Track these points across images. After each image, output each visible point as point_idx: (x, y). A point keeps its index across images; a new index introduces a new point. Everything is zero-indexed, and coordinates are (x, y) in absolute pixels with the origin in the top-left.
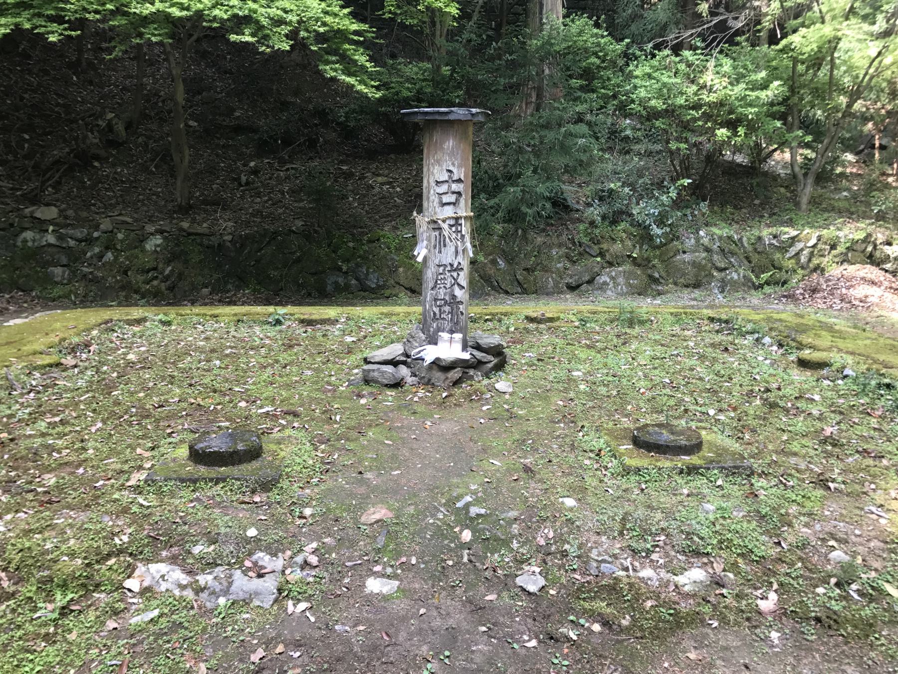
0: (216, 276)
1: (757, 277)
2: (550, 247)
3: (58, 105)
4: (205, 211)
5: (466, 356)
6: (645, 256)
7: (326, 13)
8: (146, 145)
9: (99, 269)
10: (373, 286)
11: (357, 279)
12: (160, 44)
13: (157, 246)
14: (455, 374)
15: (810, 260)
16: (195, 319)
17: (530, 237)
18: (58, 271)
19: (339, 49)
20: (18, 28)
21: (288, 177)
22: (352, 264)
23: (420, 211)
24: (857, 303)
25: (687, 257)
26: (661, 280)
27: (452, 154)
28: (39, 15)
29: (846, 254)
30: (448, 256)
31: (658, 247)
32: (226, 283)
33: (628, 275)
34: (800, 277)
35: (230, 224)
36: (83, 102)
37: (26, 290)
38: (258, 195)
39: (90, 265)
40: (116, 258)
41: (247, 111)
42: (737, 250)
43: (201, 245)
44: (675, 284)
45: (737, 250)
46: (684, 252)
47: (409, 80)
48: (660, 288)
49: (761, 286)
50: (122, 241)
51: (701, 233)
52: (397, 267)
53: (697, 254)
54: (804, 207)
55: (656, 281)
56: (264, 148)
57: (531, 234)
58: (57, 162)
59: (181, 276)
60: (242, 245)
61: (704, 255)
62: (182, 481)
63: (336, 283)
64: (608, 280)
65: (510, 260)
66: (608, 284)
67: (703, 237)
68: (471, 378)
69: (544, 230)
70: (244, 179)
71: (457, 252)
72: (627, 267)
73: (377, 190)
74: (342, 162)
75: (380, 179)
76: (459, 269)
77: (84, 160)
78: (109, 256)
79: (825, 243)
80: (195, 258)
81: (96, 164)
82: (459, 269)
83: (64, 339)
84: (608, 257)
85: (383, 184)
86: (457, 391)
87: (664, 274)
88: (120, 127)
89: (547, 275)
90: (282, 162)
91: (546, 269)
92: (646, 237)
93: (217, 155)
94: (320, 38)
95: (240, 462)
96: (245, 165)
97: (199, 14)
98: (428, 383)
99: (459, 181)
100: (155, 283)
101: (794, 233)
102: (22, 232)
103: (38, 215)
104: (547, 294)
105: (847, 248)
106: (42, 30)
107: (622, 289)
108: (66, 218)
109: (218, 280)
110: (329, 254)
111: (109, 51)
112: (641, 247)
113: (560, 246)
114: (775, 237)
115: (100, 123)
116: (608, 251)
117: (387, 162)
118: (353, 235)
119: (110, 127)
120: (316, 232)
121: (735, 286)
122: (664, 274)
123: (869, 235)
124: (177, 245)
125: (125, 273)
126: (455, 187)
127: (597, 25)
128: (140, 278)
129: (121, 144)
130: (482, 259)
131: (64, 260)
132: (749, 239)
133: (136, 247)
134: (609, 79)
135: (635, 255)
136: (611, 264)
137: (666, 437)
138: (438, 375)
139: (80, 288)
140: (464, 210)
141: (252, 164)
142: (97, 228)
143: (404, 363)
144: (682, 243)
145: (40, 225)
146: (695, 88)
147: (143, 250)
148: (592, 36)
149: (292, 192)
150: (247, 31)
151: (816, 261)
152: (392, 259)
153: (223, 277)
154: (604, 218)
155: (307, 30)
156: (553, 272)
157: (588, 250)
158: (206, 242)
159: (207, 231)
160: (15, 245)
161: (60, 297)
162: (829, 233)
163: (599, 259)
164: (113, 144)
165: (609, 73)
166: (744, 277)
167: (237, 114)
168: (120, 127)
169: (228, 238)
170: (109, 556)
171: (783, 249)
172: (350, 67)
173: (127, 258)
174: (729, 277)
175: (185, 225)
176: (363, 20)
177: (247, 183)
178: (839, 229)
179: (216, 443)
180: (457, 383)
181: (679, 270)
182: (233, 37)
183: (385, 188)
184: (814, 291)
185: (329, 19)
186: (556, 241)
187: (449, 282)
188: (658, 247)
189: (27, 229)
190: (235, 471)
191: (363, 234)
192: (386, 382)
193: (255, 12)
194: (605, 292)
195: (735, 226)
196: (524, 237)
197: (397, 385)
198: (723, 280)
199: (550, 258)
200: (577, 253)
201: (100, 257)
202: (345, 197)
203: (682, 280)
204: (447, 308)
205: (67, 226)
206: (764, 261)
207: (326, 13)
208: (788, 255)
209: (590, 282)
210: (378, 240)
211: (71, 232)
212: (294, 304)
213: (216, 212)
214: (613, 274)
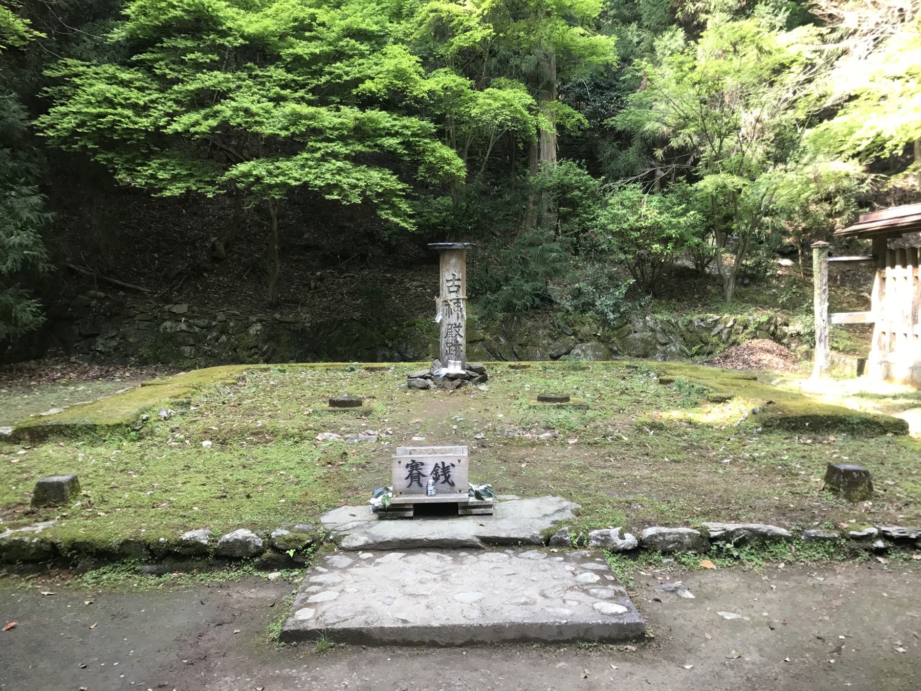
0: (299, 352)
1: (690, 350)
2: (537, 329)
3: (175, 232)
4: (289, 307)
5: (463, 372)
7: (382, 179)
8: (240, 260)
11: (399, 352)
12: (280, 200)
13: (257, 331)
14: (457, 382)
15: (729, 337)
18: (187, 349)
20: (189, 190)
21: (345, 283)
22: (396, 342)
23: (438, 296)
24: (752, 364)
25: (637, 336)
27: (455, 266)
28: (200, 181)
29: (755, 333)
30: (453, 319)
31: (616, 329)
33: (594, 349)
34: (722, 349)
35: (308, 315)
36: (192, 229)
38: (325, 296)
39: (209, 345)
40: (228, 340)
42: (674, 330)
43: (289, 330)
44: (630, 355)
45: (674, 330)
46: (635, 332)
47: (437, 210)
49: (693, 356)
51: (647, 318)
52: (428, 344)
54: (729, 299)
55: (616, 353)
56: (328, 261)
57: (524, 320)
59: (274, 351)
61: (650, 334)
65: (509, 338)
69: (533, 317)
70: (313, 285)
72: (594, 343)
73: (413, 291)
74: (387, 271)
75: (415, 283)
76: (460, 326)
77: (197, 272)
79: (739, 325)
80: (284, 339)
81: (205, 275)
84: (580, 336)
85: (419, 287)
86: (458, 390)
87: (621, 348)
88: (221, 247)
90: (341, 272)
92: (605, 322)
93: (292, 267)
94: (379, 195)
96: (312, 274)
97: (306, 184)
98: (443, 387)
99: (459, 280)
101: (716, 317)
102: (162, 323)
105: (756, 328)
106: (203, 190)
108: (193, 312)
110: (383, 332)
112: (603, 329)
113: (545, 328)
114: (702, 320)
115: (207, 244)
116: (579, 331)
117: (420, 270)
118: (396, 321)
119: (214, 247)
120: (370, 320)
121: (673, 356)
122: (621, 348)
123: (771, 319)
124: (272, 330)
125: (235, 350)
126: (456, 283)
127: (579, 166)
128: (245, 353)
131: (192, 341)
132: (683, 322)
134: (590, 206)
136: (582, 341)
138: (448, 383)
140: (462, 295)
141: (318, 273)
142: (215, 318)
143: (430, 378)
145: (176, 317)
146: (636, 217)
148: (575, 175)
149: (349, 293)
150: (335, 193)
151: (733, 338)
154: (576, 308)
155: (371, 191)
158: (292, 328)
159: (293, 320)
162: (745, 317)
164: (216, 259)
165: (590, 202)
167: (306, 236)
168: (221, 247)
171: (709, 329)
172: (397, 212)
173: (236, 340)
175: (277, 316)
176: (405, 182)
177: (315, 288)
178: (750, 315)
179: (340, 398)
180: (458, 387)
182: (327, 197)
183: (419, 289)
184: (727, 357)
185: (384, 183)
186: (541, 324)
187: (454, 333)
188: (616, 329)
189: (166, 320)
193: (340, 181)
195: (675, 313)
196: (519, 322)
197: (426, 388)
198: (664, 352)
199: (538, 337)
200: (557, 333)
202: (389, 296)
204: (453, 348)
205: (194, 318)
206: (694, 338)
207: (382, 179)
208: (713, 334)
211: (197, 322)
213: (297, 307)
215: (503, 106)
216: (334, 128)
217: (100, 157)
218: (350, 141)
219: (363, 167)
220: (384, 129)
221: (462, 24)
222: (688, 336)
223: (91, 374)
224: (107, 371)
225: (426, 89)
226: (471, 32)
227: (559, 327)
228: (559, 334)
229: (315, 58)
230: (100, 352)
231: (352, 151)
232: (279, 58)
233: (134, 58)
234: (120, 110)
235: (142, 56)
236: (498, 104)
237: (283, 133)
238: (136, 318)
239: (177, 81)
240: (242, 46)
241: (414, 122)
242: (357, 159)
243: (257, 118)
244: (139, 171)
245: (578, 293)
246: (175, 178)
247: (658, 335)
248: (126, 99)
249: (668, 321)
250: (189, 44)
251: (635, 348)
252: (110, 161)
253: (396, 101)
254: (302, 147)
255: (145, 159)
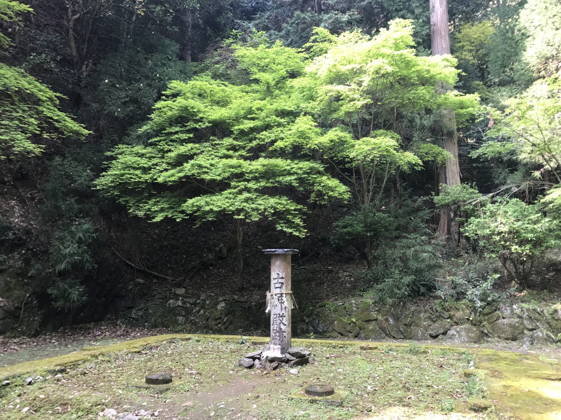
0: (246, 323)
1: (556, 336)
2: (420, 312)
6: (478, 319)
9: (197, 318)
10: (321, 331)
11: (313, 327)
13: (222, 307)
14: (275, 364)
16: (210, 339)
17: (408, 307)
18: (180, 318)
19: (286, 217)
25: (506, 321)
26: (489, 335)
27: (279, 267)
32: (250, 327)
33: (468, 331)
37: (167, 327)
40: (205, 313)
41: (286, 240)
42: (540, 318)
43: (241, 307)
44: (499, 337)
45: (540, 318)
46: (504, 318)
48: (490, 339)
50: (208, 305)
51: (514, 306)
52: (334, 321)
53: (512, 319)
58: (193, 268)
60: (260, 307)
61: (517, 320)
62: (137, 387)
63: (302, 328)
64: (455, 333)
65: (397, 319)
66: (455, 336)
67: (515, 309)
68: (283, 367)
69: (416, 303)
71: (282, 309)
72: (467, 326)
75: (345, 274)
76: (283, 316)
77: (205, 266)
78: (202, 312)
80: (238, 313)
81: (211, 268)
82: (283, 316)
83: (148, 344)
84: (455, 319)
85: (346, 276)
87: (491, 331)
89: (418, 328)
91: (418, 325)
95: (159, 384)
99: (282, 278)
100: (220, 325)
103: (177, 292)
104: (418, 340)
106: (175, 217)
107: (464, 339)
108: (188, 293)
109: (247, 325)
111: (196, 224)
113: (425, 312)
116: (454, 315)
125: (208, 320)
126: (280, 280)
127: (471, 187)
128: (214, 323)
129: (224, 258)
130: (380, 318)
131: (184, 313)
132: (548, 311)
133: (213, 308)
135: (471, 319)
136: (457, 324)
137: (318, 389)
139: (188, 326)
142: (199, 299)
144: (502, 312)
147: (217, 309)
152: (331, 316)
153: (249, 324)
156: (421, 327)
157: (442, 315)
158: (243, 306)
160: (166, 306)
161: (179, 331)
163: (449, 320)
164: (220, 258)
166: (547, 335)
167: (281, 241)
168: (225, 251)
169: (253, 304)
170: (99, 405)
172: (290, 224)
173: (209, 313)
174: (536, 335)
175: (236, 297)
179: (154, 377)
180: (275, 368)
181: (501, 328)
182: (236, 217)
186: (423, 309)
187: (278, 322)
189: (172, 299)
190: (155, 386)
191: (317, 303)
192: (246, 366)
193: (245, 206)
194: (453, 340)
198: (532, 337)
199: (419, 318)
200: (436, 317)
201: (199, 311)
203: (503, 335)
204: (278, 334)
209: (445, 333)
210: (325, 306)
212: (257, 335)
214: (458, 329)
215: (373, 149)
216: (251, 172)
217: (121, 200)
218: (261, 180)
219: (266, 196)
220: (285, 170)
221: (348, 97)
222: (554, 323)
223: (118, 333)
224: (127, 332)
225: (316, 142)
226: (354, 102)
227: (437, 311)
228: (437, 317)
229: (252, 130)
230: (133, 318)
231: (260, 186)
232: (232, 132)
233: (151, 141)
234: (132, 171)
235: (154, 140)
236: (370, 148)
237: (219, 178)
238: (155, 297)
239: (170, 151)
240: (207, 127)
241: (305, 165)
242: (263, 192)
243: (205, 170)
244: (142, 207)
245: (455, 286)
246: (162, 210)
247: (525, 322)
248: (138, 165)
249: (534, 310)
250: (178, 129)
251: (503, 332)
252: (127, 202)
253: (296, 152)
254: (228, 186)
255: (147, 200)
